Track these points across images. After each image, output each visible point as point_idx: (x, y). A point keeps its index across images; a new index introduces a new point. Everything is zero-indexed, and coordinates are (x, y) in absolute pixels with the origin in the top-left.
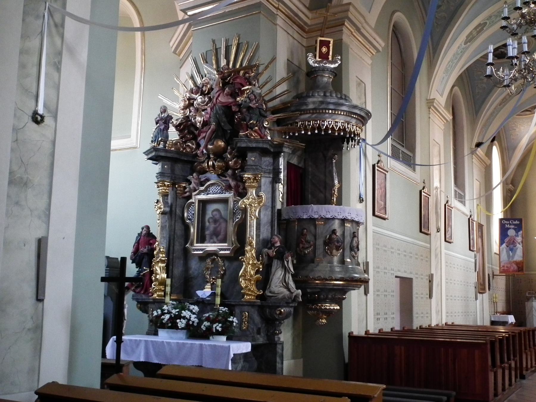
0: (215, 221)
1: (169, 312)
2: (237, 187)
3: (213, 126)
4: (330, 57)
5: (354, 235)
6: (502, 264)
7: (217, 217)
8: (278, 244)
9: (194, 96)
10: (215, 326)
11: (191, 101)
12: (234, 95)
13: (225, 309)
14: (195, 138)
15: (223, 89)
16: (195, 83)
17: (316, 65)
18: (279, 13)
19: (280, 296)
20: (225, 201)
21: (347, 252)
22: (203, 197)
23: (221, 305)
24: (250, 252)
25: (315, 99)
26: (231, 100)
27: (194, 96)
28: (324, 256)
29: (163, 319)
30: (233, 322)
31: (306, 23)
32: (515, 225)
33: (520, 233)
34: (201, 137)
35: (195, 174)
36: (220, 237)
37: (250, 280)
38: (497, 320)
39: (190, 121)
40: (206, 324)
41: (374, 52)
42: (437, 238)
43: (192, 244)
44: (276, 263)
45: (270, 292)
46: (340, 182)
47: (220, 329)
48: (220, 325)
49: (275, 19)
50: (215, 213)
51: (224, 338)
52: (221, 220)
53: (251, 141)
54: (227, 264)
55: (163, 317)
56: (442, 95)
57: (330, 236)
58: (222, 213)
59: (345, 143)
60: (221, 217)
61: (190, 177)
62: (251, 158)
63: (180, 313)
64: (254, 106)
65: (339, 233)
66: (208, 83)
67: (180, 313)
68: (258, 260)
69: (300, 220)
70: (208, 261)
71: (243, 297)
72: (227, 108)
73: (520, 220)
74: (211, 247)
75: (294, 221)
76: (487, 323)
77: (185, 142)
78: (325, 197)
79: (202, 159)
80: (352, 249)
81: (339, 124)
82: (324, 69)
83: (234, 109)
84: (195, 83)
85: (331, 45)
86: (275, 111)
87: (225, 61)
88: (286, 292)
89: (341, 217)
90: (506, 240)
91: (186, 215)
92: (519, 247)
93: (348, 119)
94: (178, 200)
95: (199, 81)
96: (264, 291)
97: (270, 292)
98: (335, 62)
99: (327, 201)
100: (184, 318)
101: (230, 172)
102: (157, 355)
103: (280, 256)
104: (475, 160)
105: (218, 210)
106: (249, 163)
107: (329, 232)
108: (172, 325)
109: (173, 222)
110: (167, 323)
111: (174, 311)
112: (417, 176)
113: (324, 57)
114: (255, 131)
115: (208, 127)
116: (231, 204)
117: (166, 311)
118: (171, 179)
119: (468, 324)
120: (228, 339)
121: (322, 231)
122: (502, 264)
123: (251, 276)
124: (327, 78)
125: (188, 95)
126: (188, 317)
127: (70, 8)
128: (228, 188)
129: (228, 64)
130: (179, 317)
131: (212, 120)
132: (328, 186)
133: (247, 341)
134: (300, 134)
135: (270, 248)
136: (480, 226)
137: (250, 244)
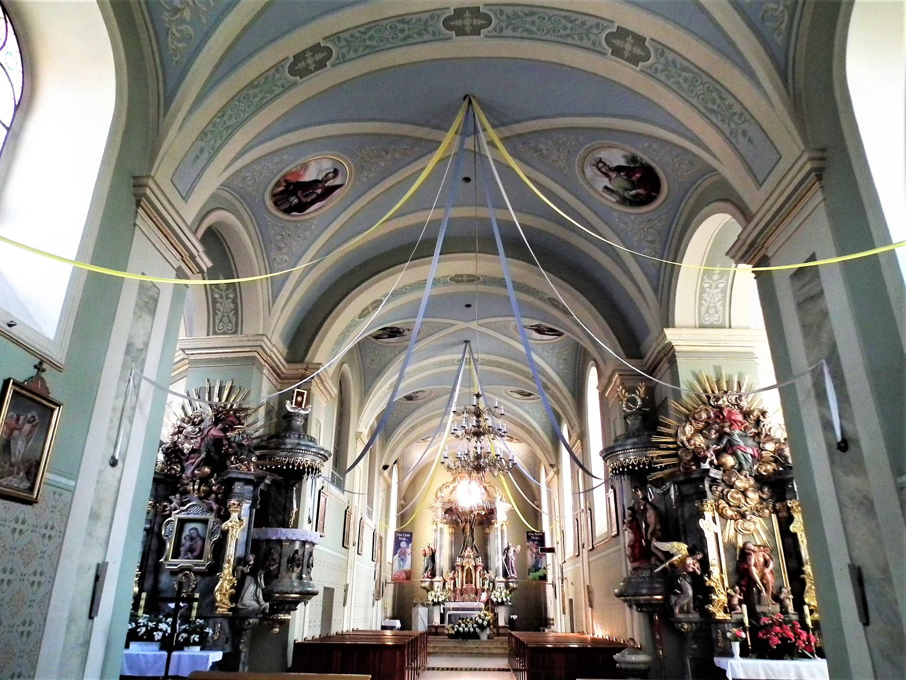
0: (192, 539)
1: (146, 626)
2: (219, 510)
3: (203, 456)
4: (303, 405)
5: (311, 555)
6: (394, 573)
7: (194, 535)
8: (252, 562)
9: (185, 425)
10: (192, 637)
11: (181, 429)
12: (224, 430)
13: (201, 621)
14: (181, 462)
15: (216, 423)
16: (186, 414)
17: (292, 411)
18: (266, 365)
19: (251, 608)
20: (205, 522)
21: (305, 568)
22: (183, 516)
23: (196, 618)
24: (227, 569)
25: (292, 441)
26: (222, 434)
27: (185, 425)
28: (287, 573)
29: (139, 632)
30: (208, 633)
31: (283, 373)
32: (407, 538)
33: (410, 545)
34: (188, 462)
35: (178, 495)
36: (196, 554)
37: (225, 595)
38: (386, 625)
39: (178, 446)
40: (184, 635)
41: (328, 397)
42: (353, 549)
43: (166, 559)
44: (249, 579)
45: (242, 605)
46: (298, 506)
47: (197, 640)
48: (198, 636)
49: (263, 369)
50: (192, 531)
51: (198, 648)
52: (198, 539)
53: (240, 473)
54: (199, 578)
55: (139, 630)
56: (366, 428)
57: (294, 555)
58: (200, 531)
59: (306, 474)
60: (198, 535)
61: (172, 497)
62: (238, 487)
63: (157, 625)
64: (246, 444)
65: (300, 553)
66: (199, 416)
67: (157, 625)
68: (234, 576)
69: (269, 541)
70: (180, 575)
71: (216, 609)
72: (217, 442)
73: (411, 534)
74: (182, 562)
75: (263, 541)
76: (379, 628)
77: (170, 465)
78: (284, 518)
79: (186, 482)
80: (308, 566)
81: (309, 463)
82: (298, 415)
83: (225, 442)
84: (186, 414)
85: (305, 396)
86: (257, 448)
87: (218, 399)
88: (256, 605)
89: (303, 539)
90: (399, 551)
91: (163, 533)
92: (409, 557)
93: (316, 458)
94: (157, 517)
95: (190, 413)
96: (236, 604)
97: (242, 605)
98: (307, 410)
99: (285, 525)
100: (161, 630)
101: (213, 496)
102: (130, 668)
103: (254, 573)
104: (381, 481)
105: (196, 529)
106: (235, 491)
107: (293, 552)
108: (149, 637)
109: (149, 538)
110: (143, 635)
111: (150, 624)
112: (345, 497)
113: (299, 404)
114: (245, 465)
115: (197, 455)
116: (210, 525)
117: (142, 624)
118: (155, 499)
119: (366, 629)
120: (201, 649)
121: (287, 551)
122: (394, 573)
123: (227, 591)
124: (299, 422)
125: (179, 423)
126: (164, 629)
127: (145, 374)
128: (211, 510)
129: (220, 400)
130: (156, 629)
131: (203, 449)
132: (287, 509)
133: (218, 650)
134: (276, 467)
135: (244, 566)
136: (381, 538)
137: (229, 562)
